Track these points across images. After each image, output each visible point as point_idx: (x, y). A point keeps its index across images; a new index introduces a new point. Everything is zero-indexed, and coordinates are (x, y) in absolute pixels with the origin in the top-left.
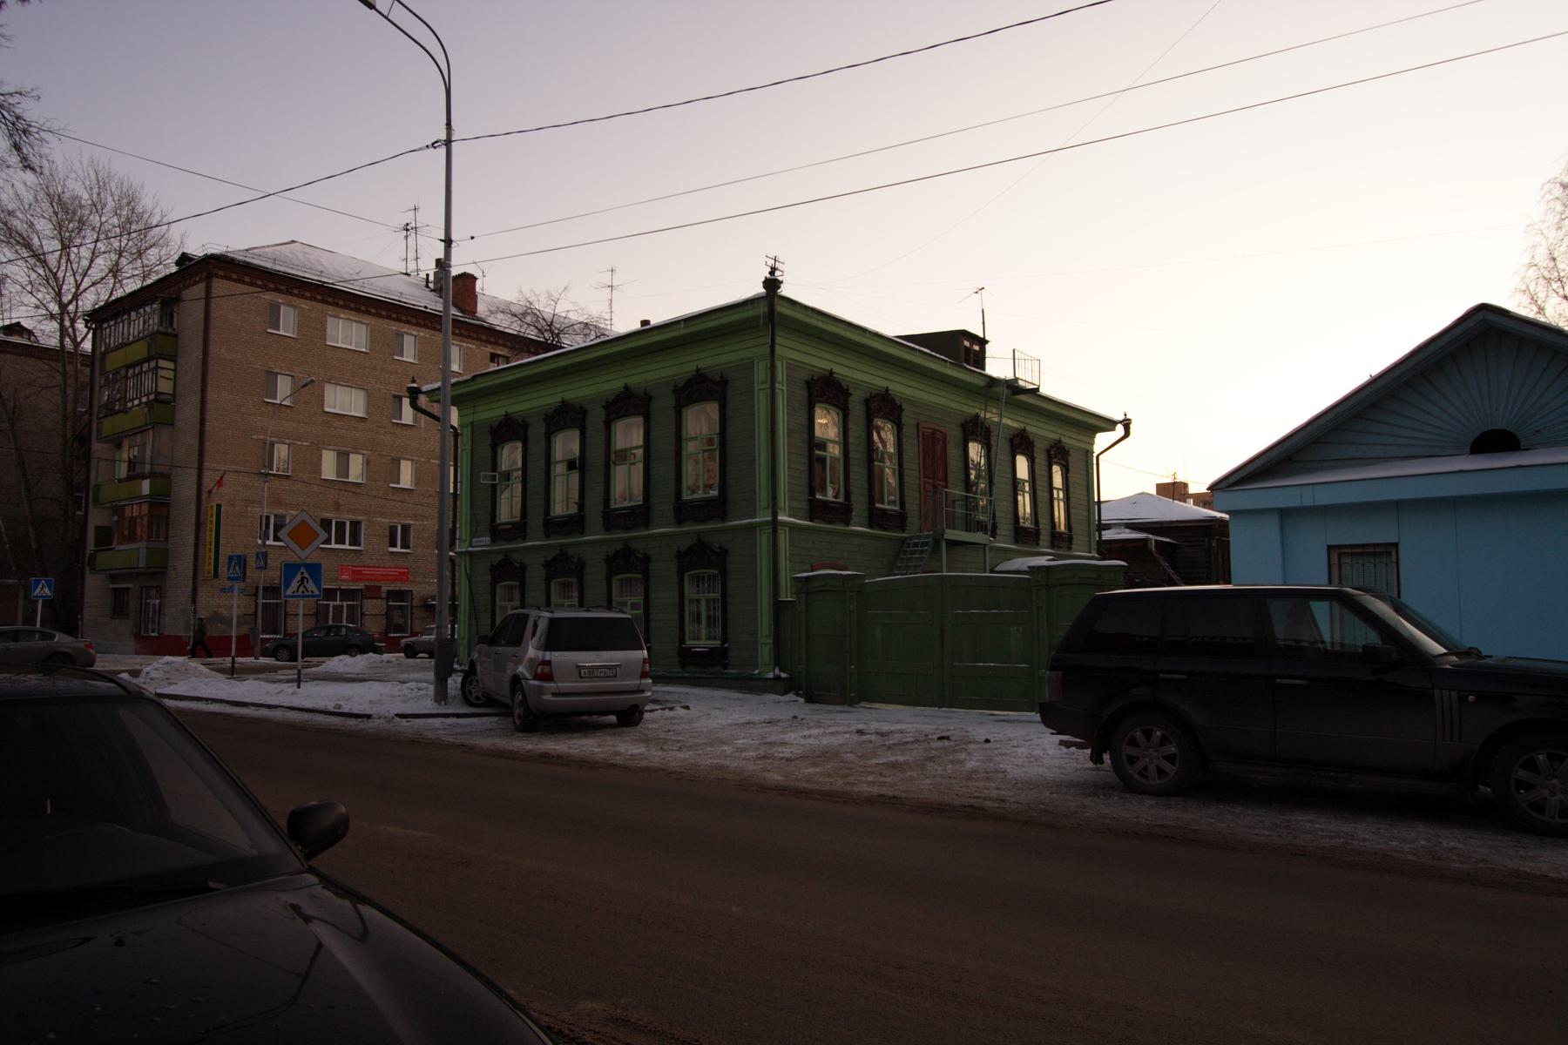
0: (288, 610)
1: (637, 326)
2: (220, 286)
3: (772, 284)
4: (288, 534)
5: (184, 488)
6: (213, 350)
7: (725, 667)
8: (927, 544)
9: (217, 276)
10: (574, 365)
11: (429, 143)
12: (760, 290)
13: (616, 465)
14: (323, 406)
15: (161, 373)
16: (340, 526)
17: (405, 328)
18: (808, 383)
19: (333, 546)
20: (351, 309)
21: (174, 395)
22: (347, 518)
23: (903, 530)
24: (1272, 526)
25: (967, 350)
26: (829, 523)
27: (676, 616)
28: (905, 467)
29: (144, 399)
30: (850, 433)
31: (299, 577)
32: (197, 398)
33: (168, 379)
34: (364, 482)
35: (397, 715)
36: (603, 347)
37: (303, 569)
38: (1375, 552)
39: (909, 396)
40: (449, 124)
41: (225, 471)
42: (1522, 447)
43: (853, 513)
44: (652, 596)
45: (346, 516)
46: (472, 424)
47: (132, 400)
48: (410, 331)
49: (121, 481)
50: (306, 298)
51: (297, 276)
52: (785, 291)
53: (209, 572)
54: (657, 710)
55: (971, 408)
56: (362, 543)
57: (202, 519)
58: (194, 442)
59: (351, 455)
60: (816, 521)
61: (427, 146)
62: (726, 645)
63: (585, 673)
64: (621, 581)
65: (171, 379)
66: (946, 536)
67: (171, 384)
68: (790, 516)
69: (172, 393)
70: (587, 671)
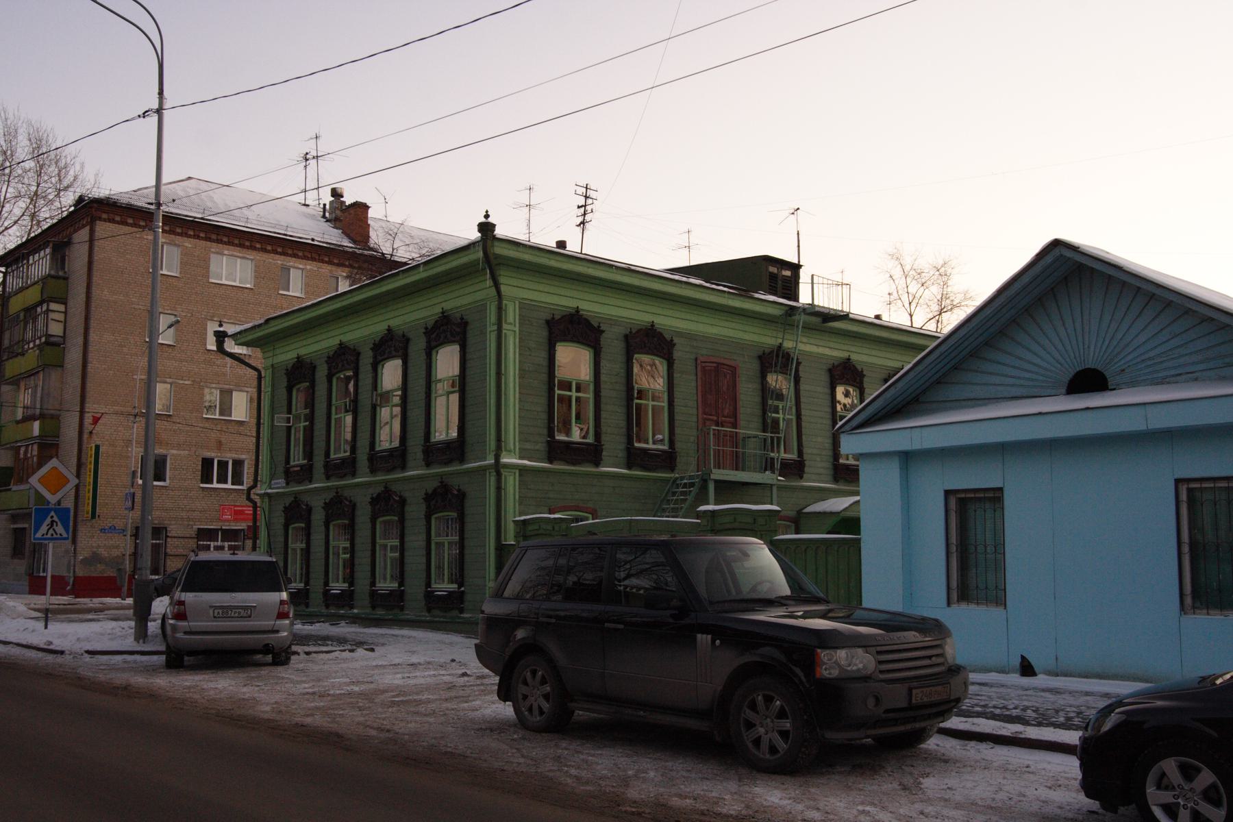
0: (168, 550)
1: (551, 243)
2: (103, 228)
3: (486, 228)
4: (69, 481)
5: (69, 432)
6: (95, 291)
7: (462, 611)
8: (692, 485)
9: (100, 219)
10: (342, 309)
11: (141, 113)
12: (475, 235)
13: (381, 407)
14: (206, 345)
15: (52, 315)
16: (223, 465)
17: (291, 262)
18: (548, 322)
19: (215, 485)
20: (236, 245)
21: (64, 337)
22: (229, 457)
23: (672, 470)
24: (893, 470)
25: (773, 277)
26: (574, 464)
27: (424, 560)
28: (675, 403)
29: (38, 342)
30: (603, 371)
31: (48, 520)
32: (80, 340)
33: (58, 321)
34: (247, 420)
35: (88, 652)
36: (375, 287)
37: (52, 513)
38: (985, 497)
39: (683, 329)
40: (161, 93)
41: (103, 414)
42: (1110, 388)
43: (604, 453)
44: (406, 539)
45: (229, 455)
46: (272, 365)
47: (29, 343)
48: (296, 265)
49: (18, 422)
50: (190, 236)
51: (180, 215)
52: (499, 232)
53: (88, 513)
54: (336, 651)
55: (768, 339)
56: (245, 483)
57: (83, 460)
58: (78, 382)
59: (234, 393)
60: (555, 462)
61: (139, 116)
62: (463, 589)
63: (218, 613)
64: (385, 522)
65: (61, 322)
66: (713, 477)
67: (61, 326)
68: (521, 458)
69: (62, 334)
70: (220, 611)
